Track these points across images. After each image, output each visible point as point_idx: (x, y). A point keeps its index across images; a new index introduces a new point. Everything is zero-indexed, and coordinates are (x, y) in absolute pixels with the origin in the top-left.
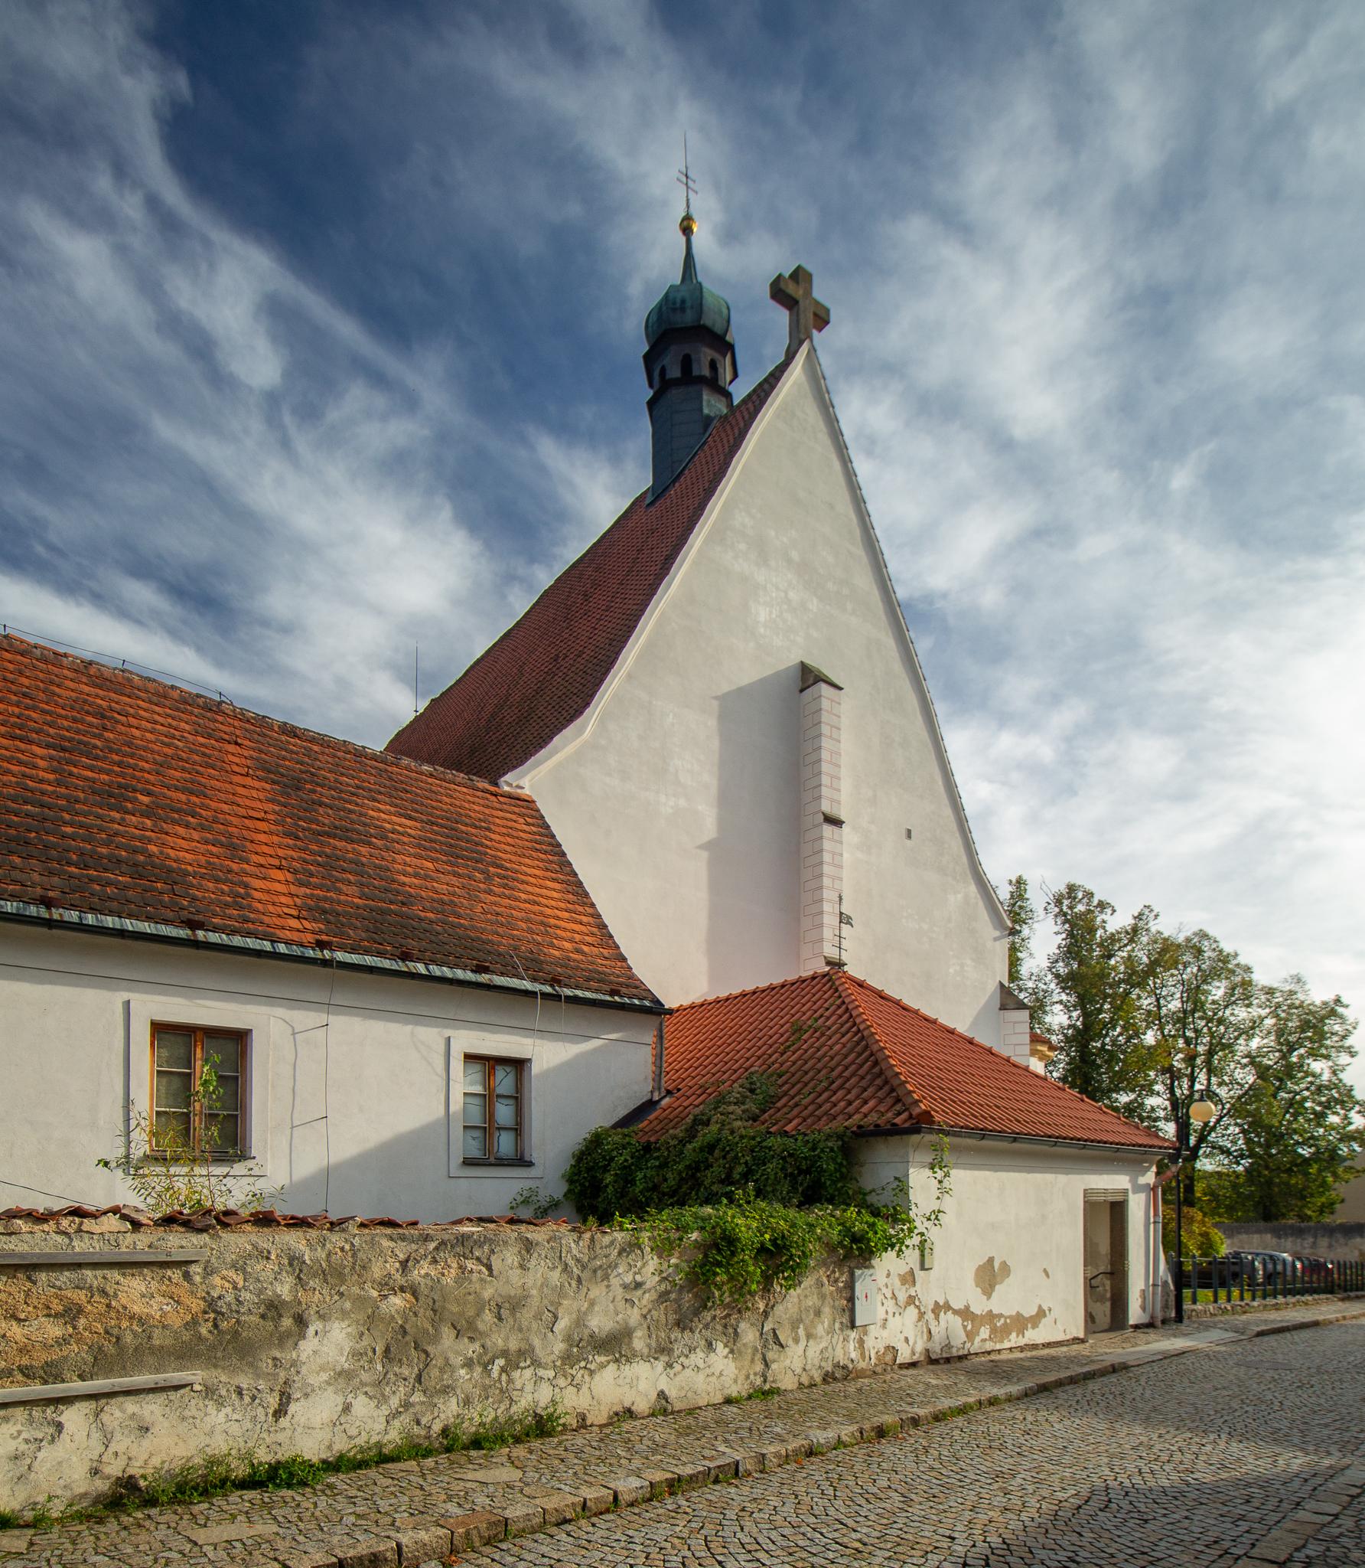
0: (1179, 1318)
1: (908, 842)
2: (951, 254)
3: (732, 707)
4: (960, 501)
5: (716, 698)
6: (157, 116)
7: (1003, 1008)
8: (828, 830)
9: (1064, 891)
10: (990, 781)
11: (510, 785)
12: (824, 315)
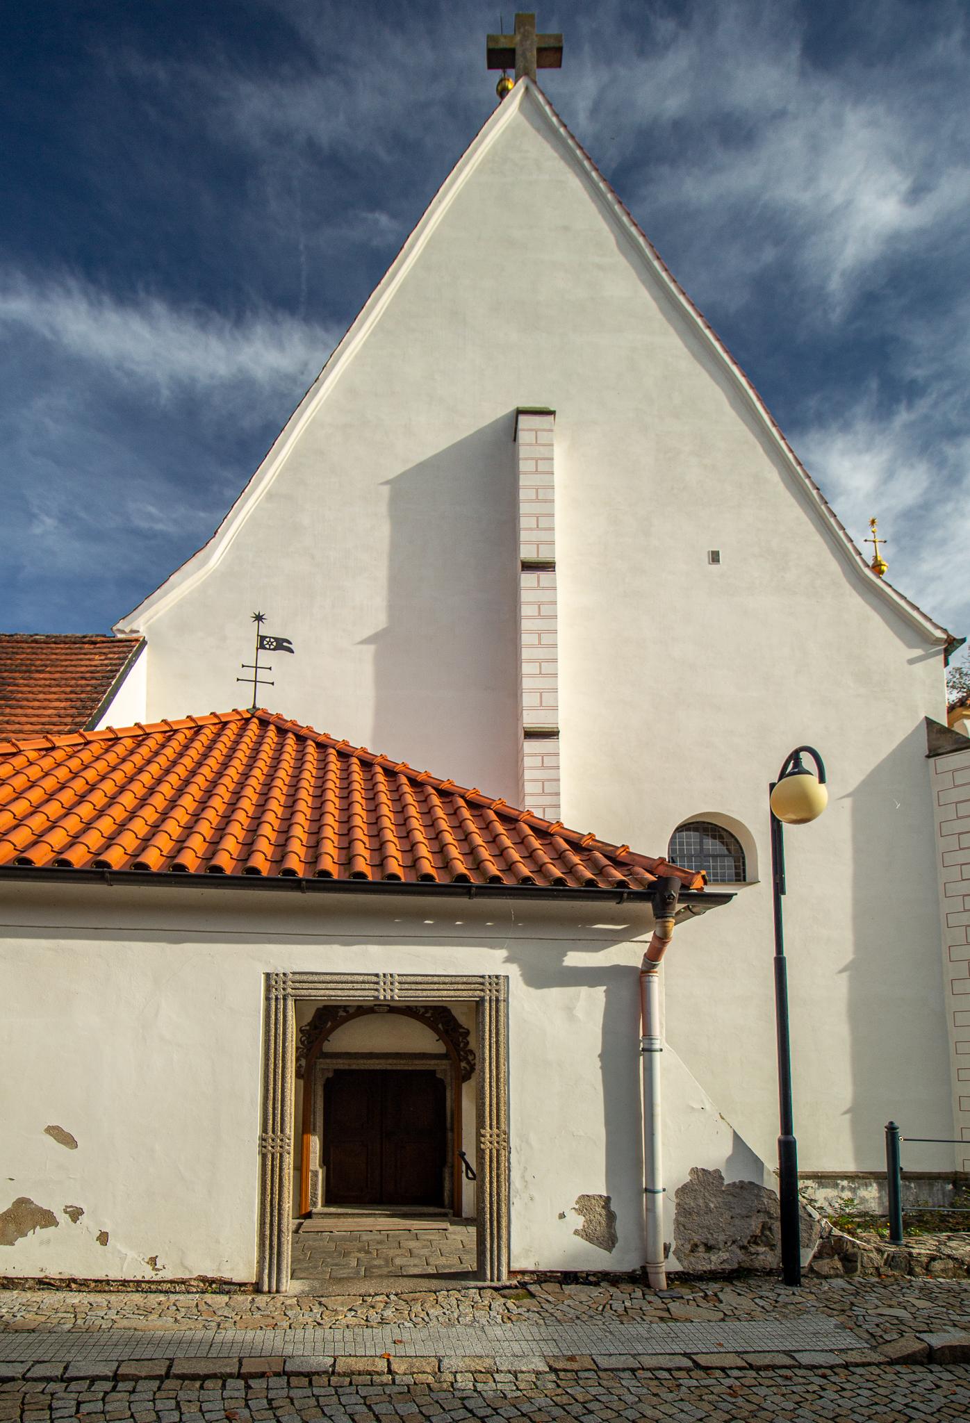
1: (714, 567)
5: (387, 483)
7: (933, 753)
11: (123, 632)
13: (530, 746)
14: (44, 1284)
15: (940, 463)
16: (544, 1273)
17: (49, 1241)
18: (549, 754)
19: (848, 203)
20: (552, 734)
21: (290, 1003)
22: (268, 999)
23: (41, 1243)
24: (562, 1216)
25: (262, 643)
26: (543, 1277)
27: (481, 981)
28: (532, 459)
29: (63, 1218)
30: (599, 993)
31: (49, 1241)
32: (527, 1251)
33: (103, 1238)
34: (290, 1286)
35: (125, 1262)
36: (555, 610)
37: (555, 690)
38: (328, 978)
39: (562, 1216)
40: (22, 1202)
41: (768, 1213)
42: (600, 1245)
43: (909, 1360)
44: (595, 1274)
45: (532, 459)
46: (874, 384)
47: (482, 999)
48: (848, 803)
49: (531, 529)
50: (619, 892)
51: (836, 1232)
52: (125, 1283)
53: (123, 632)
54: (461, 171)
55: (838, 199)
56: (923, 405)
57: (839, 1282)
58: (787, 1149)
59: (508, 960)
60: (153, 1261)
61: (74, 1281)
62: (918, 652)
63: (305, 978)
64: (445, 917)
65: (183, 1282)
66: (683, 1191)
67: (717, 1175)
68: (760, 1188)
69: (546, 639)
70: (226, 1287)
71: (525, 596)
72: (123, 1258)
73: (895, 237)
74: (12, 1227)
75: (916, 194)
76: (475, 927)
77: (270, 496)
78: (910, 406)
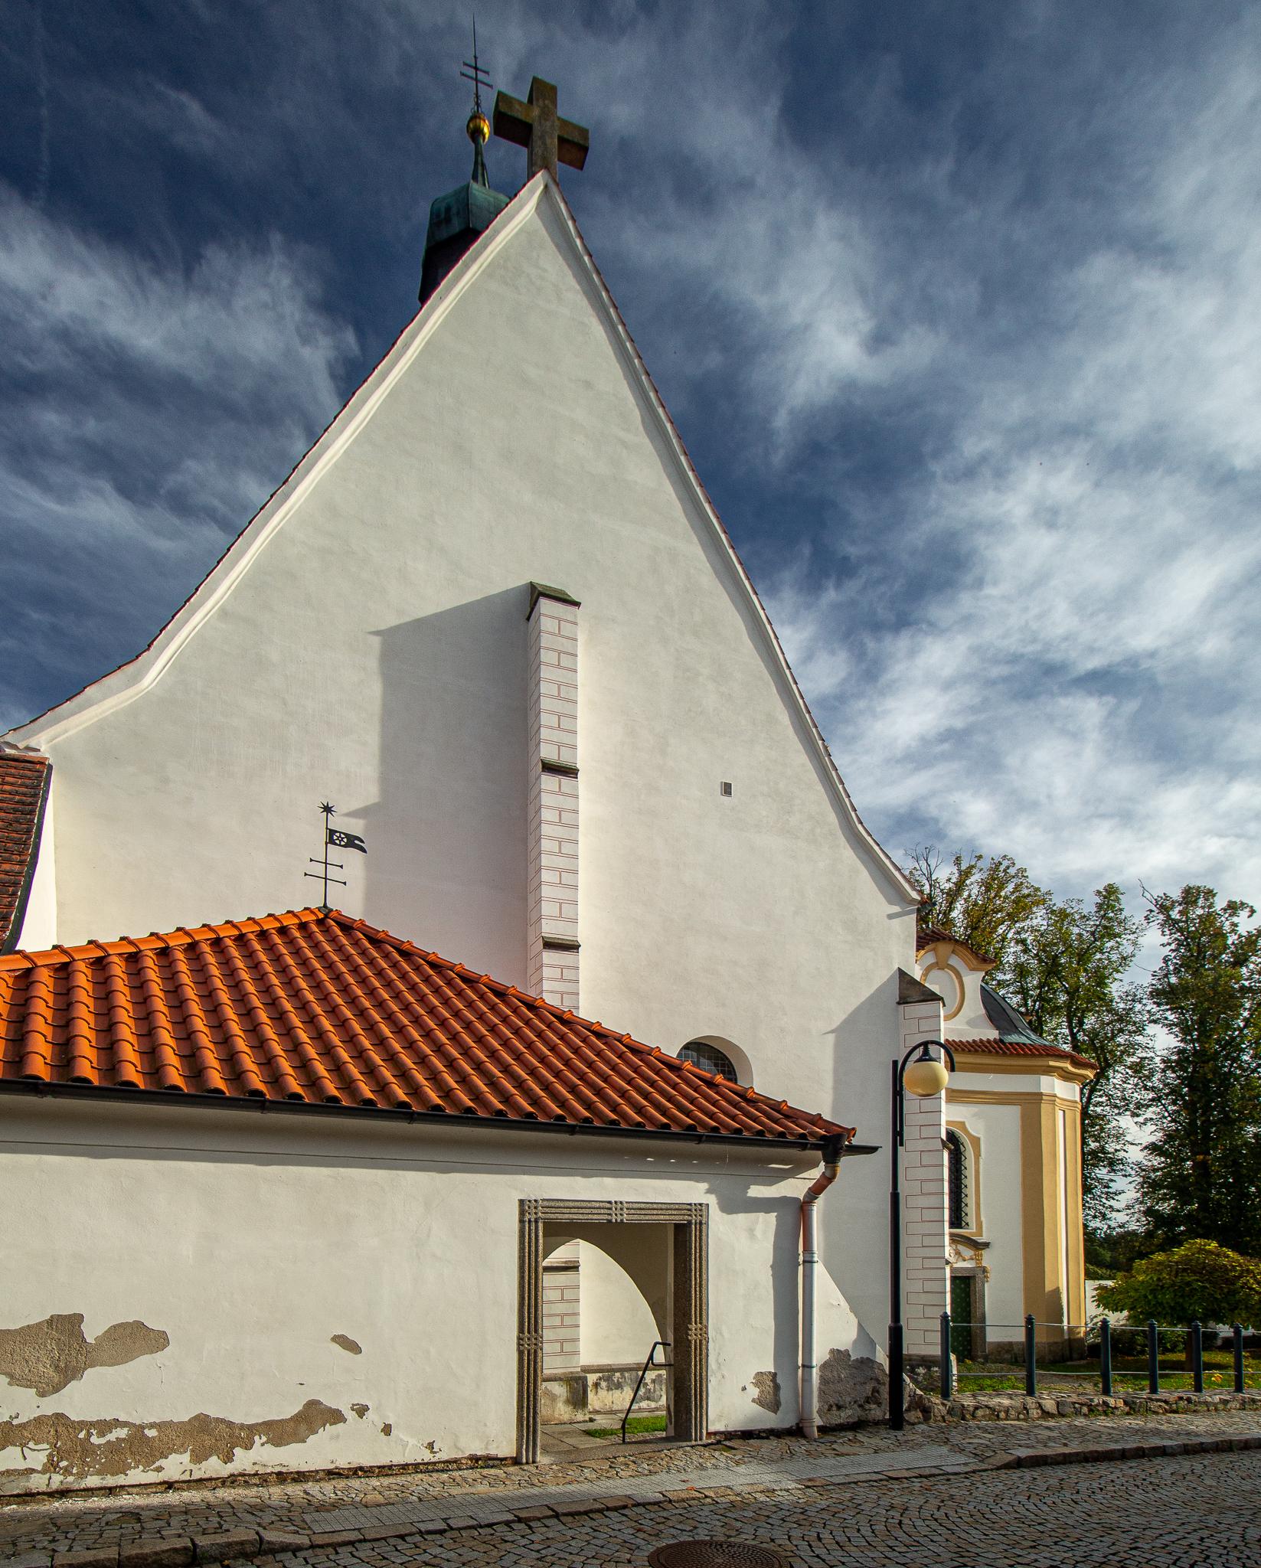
0: (896, 1421)
1: (726, 798)
2: (1151, 285)
3: (406, 649)
4: (1169, 551)
5: (377, 633)
6: (333, 376)
7: (903, 1001)
8: (549, 782)
9: (1176, 894)
10: (1220, 835)
11: (15, 747)
12: (577, 139)
13: (549, 957)
14: (333, 1474)
15: (859, 654)
16: (730, 1433)
17: (338, 1436)
18: (568, 967)
19: (807, 327)
20: (572, 947)
21: (541, 1225)
22: (522, 1221)
23: (331, 1438)
24: (744, 1389)
25: (332, 837)
26: (729, 1435)
27: (689, 1208)
28: (554, 650)
29: (350, 1415)
30: (772, 1217)
31: (338, 1436)
32: (720, 1417)
33: (387, 1430)
34: (543, 1459)
35: (407, 1449)
36: (577, 819)
37: (575, 903)
38: (571, 1204)
39: (744, 1389)
40: (313, 1405)
41: (877, 1380)
42: (769, 1409)
43: (1007, 1466)
44: (764, 1431)
45: (554, 650)
46: (806, 550)
47: (690, 1222)
48: (831, 1038)
49: (551, 728)
50: (802, 1143)
51: (919, 1392)
52: (404, 1467)
53: (15, 747)
54: (467, 267)
55: (796, 317)
56: (852, 587)
57: (923, 1427)
58: (896, 1334)
59: (708, 1191)
60: (431, 1446)
61: (361, 1468)
62: (896, 909)
63: (553, 1204)
64: (663, 1156)
65: (455, 1461)
66: (825, 1366)
67: (846, 1354)
68: (873, 1362)
69: (567, 848)
70: (491, 1463)
71: (546, 799)
72: (405, 1446)
73: (849, 386)
74: (303, 1427)
75: (879, 341)
76: (684, 1166)
77: (224, 614)
78: (838, 586)
